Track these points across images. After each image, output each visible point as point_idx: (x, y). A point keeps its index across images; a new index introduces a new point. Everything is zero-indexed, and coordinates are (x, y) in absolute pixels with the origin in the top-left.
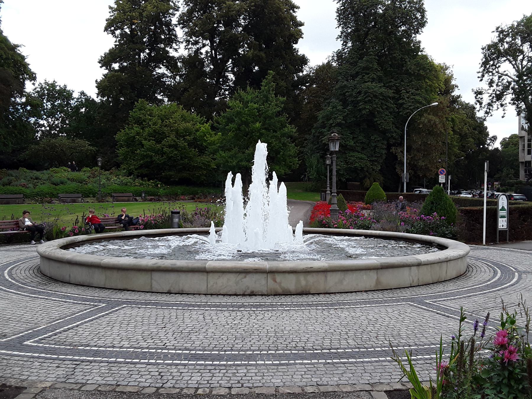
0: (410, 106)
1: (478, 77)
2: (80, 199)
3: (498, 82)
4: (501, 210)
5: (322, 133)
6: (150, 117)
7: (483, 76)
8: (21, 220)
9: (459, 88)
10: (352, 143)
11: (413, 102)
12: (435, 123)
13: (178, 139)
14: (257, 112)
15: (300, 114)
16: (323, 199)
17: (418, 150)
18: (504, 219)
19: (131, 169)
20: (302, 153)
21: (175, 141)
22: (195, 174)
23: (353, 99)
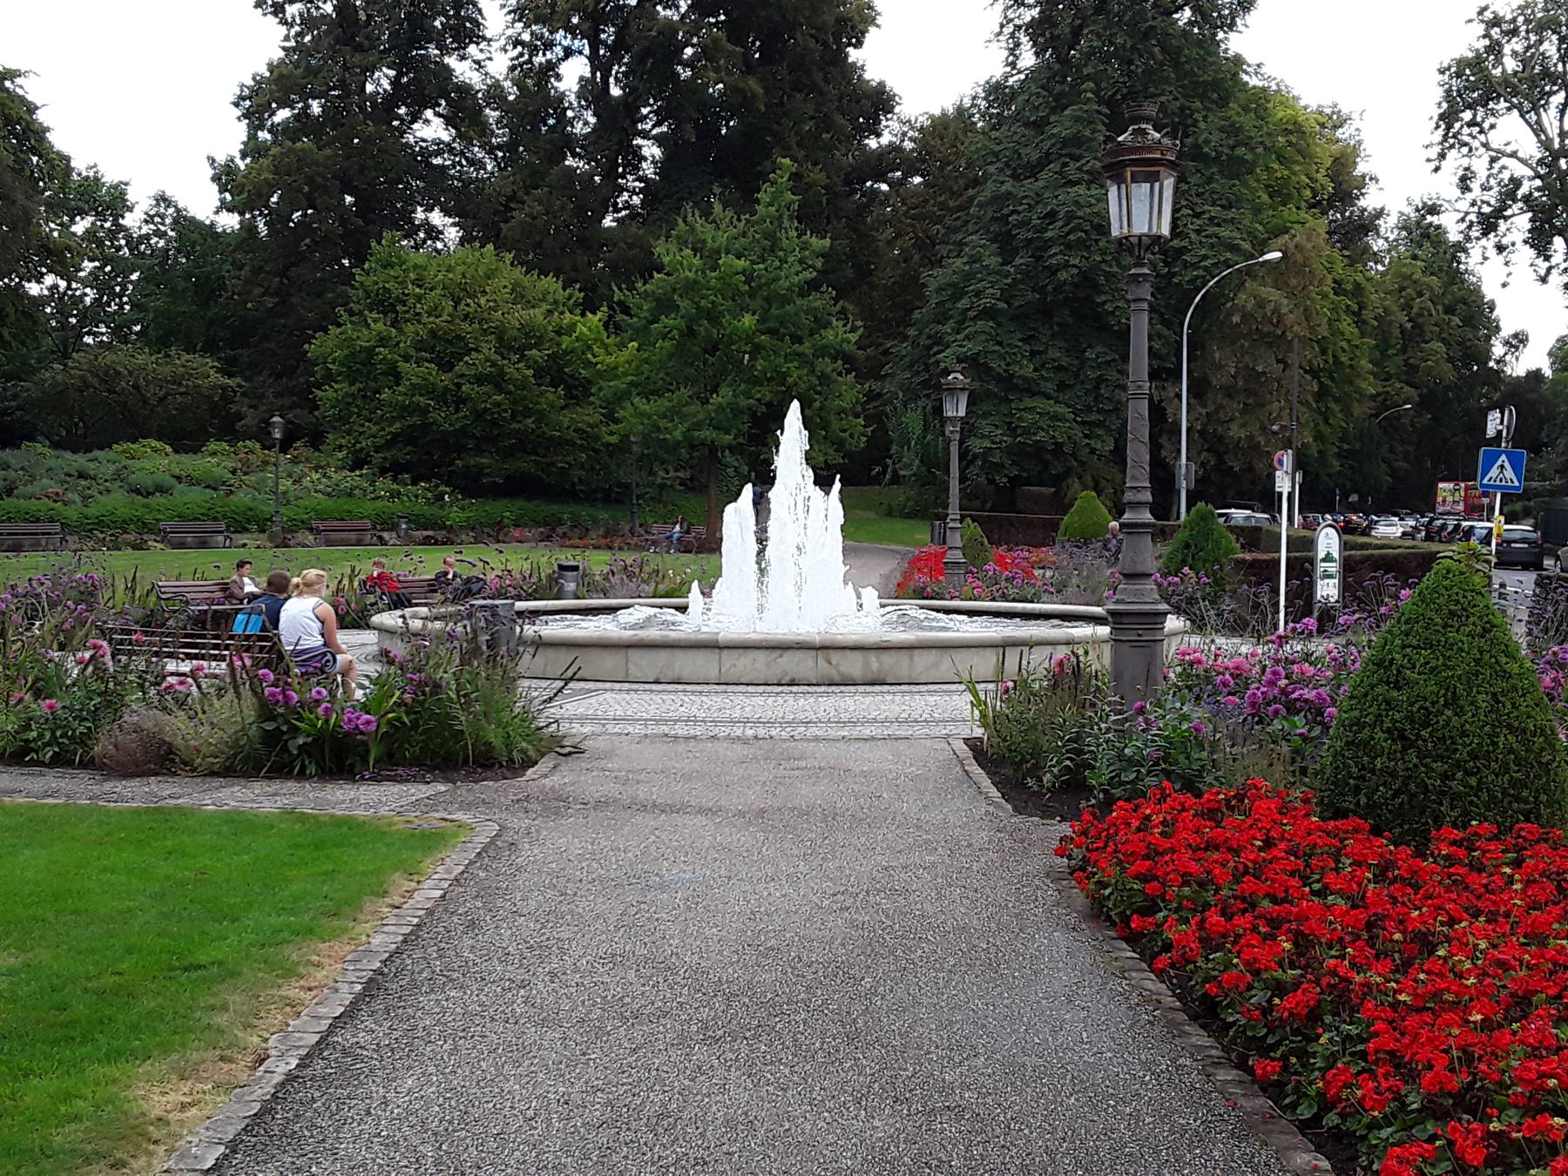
0: (1205, 257)
1: (1429, 160)
2: (220, 538)
3: (1489, 176)
4: (1323, 560)
5: (938, 340)
6: (418, 290)
7: (1442, 156)
8: (235, 582)
9: (1381, 184)
10: (1028, 370)
11: (1212, 246)
12: (1276, 311)
13: (504, 358)
14: (745, 283)
15: (871, 272)
16: (936, 541)
17: (1229, 392)
18: (1331, 582)
19: (362, 449)
20: (879, 395)
21: (494, 364)
22: (553, 464)
23: (1030, 235)
